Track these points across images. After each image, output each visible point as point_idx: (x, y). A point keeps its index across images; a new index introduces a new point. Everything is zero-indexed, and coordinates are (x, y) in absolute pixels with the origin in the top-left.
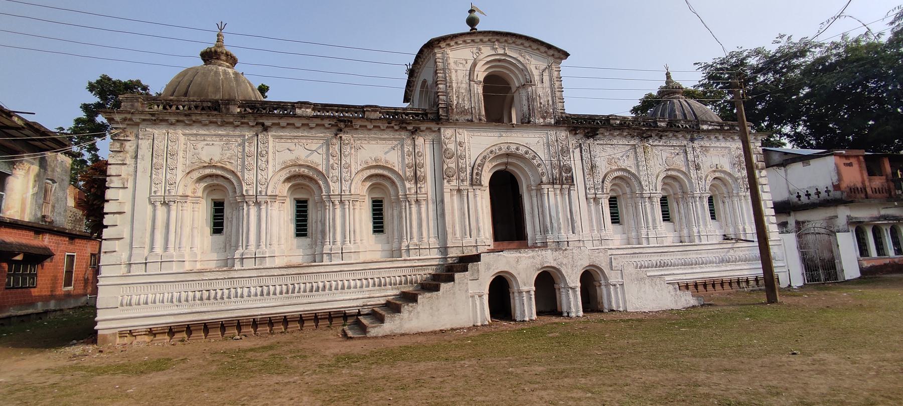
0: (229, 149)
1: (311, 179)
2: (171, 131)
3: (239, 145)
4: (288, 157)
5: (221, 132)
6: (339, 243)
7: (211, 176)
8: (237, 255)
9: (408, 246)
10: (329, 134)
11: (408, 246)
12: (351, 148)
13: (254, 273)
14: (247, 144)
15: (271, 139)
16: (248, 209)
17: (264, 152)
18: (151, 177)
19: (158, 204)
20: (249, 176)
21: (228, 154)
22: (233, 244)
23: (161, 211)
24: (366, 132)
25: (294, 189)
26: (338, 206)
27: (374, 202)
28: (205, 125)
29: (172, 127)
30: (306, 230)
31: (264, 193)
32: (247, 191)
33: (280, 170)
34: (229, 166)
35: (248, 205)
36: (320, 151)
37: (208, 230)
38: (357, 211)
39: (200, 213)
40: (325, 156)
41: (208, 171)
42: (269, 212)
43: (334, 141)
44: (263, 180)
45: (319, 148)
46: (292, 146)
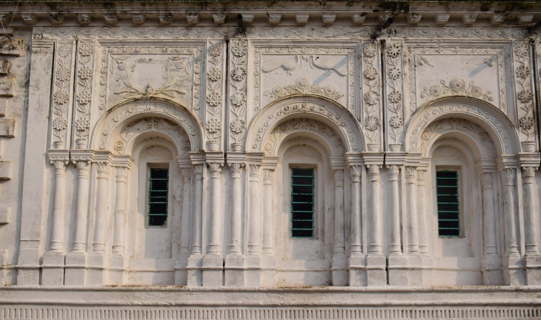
0: (178, 68)
1: (322, 125)
2: (81, 37)
3: (196, 61)
4: (283, 82)
5: (164, 35)
7: (146, 119)
8: (192, 264)
9: (523, 262)
10: (359, 37)
11: (523, 262)
13: (222, 299)
14: (209, 58)
15: (251, 49)
16: (212, 179)
17: (239, 73)
18: (49, 118)
19: (60, 166)
20: (213, 117)
21: (176, 77)
22: (184, 243)
23: (65, 178)
24: (433, 31)
25: (292, 144)
27: (439, 174)
28: (138, 25)
29: (83, 30)
30: (310, 225)
31: (239, 149)
32: (209, 143)
33: (269, 106)
34: (177, 100)
36: (342, 70)
37: (141, 218)
38: (414, 187)
39: (128, 188)
40: (351, 80)
41: (142, 109)
42: (248, 184)
43: (371, 49)
44: (238, 125)
45: (341, 64)
46: (290, 62)
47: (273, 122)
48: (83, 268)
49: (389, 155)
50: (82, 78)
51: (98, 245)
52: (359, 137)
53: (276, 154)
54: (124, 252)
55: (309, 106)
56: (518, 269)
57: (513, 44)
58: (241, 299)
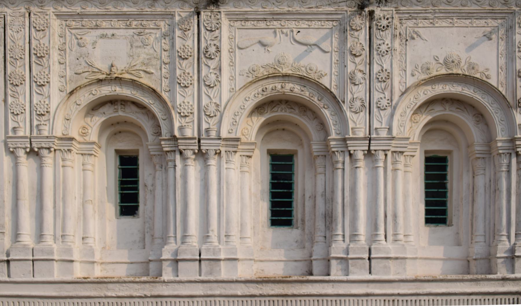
0: (145, 45)
3: (164, 36)
4: (260, 59)
6: (363, 239)
12: (394, 36)
13: (199, 290)
14: (178, 33)
15: (225, 23)
17: (212, 50)
18: (5, 101)
19: (21, 153)
20: (184, 100)
21: (143, 54)
22: (158, 233)
25: (270, 128)
26: (361, 164)
27: (428, 160)
31: (213, 134)
32: (181, 128)
34: (145, 80)
35: (184, 158)
37: (111, 208)
38: (400, 174)
39: (93, 177)
41: (106, 91)
42: (224, 172)
43: (358, 21)
44: (212, 108)
45: (324, 39)
46: (268, 37)
47: (250, 105)
48: (53, 260)
49: (375, 139)
50: (39, 56)
51: (66, 237)
52: (343, 120)
53: (253, 140)
54: (95, 243)
55: (289, 86)
56: (507, 257)
57: (517, 14)
58: (218, 290)
